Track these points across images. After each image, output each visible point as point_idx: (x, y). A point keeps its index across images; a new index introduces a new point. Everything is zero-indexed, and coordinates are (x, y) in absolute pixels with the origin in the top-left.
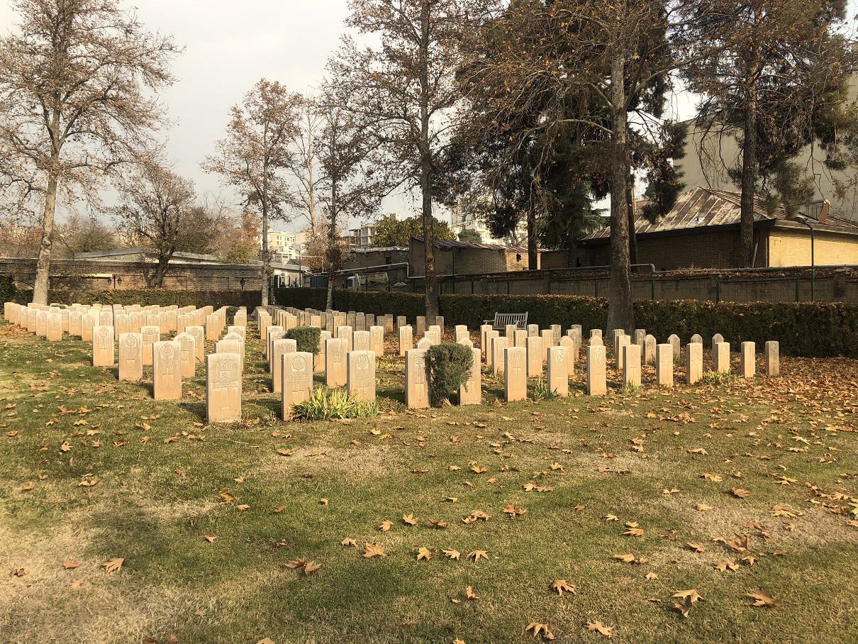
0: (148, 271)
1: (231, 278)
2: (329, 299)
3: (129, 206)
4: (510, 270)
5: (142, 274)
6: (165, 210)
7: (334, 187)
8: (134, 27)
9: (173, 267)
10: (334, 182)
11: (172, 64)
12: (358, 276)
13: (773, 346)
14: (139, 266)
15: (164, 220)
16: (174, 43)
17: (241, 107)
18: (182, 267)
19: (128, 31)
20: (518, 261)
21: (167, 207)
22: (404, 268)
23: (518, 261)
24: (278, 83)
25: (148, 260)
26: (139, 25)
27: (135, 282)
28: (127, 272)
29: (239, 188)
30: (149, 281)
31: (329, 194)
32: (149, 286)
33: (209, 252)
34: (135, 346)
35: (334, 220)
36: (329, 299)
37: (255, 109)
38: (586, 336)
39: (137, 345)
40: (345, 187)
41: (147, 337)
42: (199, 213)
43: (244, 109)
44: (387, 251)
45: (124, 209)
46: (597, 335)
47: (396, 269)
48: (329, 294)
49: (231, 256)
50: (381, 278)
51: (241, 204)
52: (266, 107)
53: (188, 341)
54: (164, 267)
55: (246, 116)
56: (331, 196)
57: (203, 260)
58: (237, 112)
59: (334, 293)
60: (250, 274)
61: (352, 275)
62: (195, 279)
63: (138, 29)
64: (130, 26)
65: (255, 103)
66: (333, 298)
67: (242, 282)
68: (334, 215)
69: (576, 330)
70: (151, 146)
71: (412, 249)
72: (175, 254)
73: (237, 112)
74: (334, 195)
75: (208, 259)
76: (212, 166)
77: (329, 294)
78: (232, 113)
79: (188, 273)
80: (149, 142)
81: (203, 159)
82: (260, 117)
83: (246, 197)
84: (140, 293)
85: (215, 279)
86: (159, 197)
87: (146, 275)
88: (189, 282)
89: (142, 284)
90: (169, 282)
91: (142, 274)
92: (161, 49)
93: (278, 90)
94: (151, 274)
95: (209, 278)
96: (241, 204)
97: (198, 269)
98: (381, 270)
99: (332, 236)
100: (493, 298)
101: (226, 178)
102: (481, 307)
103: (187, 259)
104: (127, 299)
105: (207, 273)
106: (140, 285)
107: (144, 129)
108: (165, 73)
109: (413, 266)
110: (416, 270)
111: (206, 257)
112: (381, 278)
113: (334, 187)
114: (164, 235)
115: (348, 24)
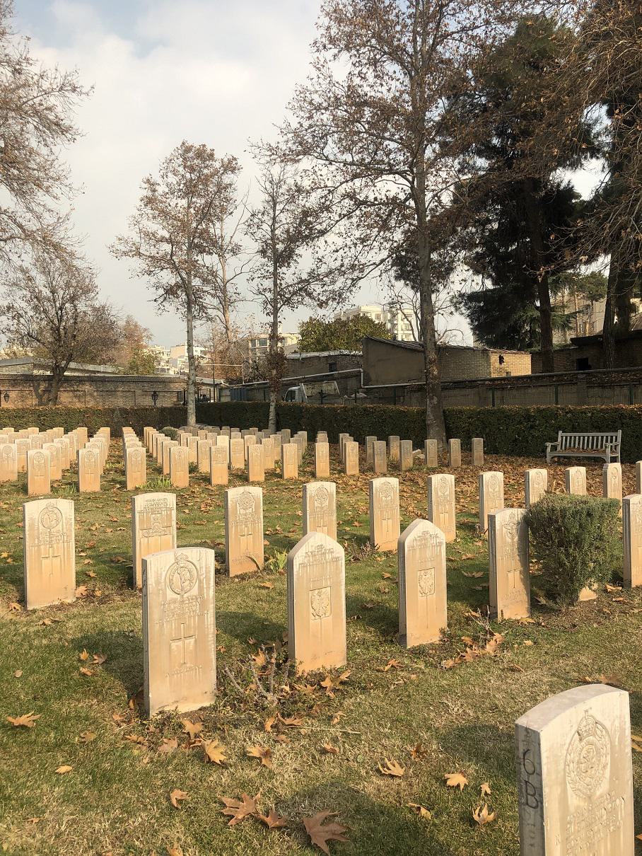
0: (39, 385)
1: (138, 392)
2: (272, 415)
3: (15, 305)
4: (493, 376)
5: (31, 389)
6: (61, 309)
7: (275, 275)
8: (24, 65)
9: (68, 379)
10: (276, 269)
11: (73, 111)
12: (303, 386)
13: (478, 443)
14: (28, 379)
15: (60, 321)
16: (79, 81)
17: (156, 178)
18: (80, 381)
19: (17, 71)
20: (500, 363)
21: (64, 304)
22: (357, 375)
23: (500, 363)
24: (204, 146)
25: (35, 372)
26: (31, 62)
27: (23, 398)
28: (13, 386)
29: (153, 280)
30: (40, 397)
31: (269, 283)
32: (41, 404)
33: (103, 362)
34: (195, 591)
35: (276, 317)
36: (272, 415)
37: (172, 179)
38: (312, 439)
39: (201, 589)
40: (289, 275)
41: (149, 519)
42: (100, 312)
43: (159, 181)
44: (330, 356)
45: (9, 308)
46: (322, 436)
47: (347, 377)
48: (272, 409)
49: (133, 367)
50: (329, 388)
51: (155, 300)
52: (188, 175)
53: (329, 557)
54: (57, 379)
55: (161, 189)
56: (272, 286)
57: (98, 372)
58: (151, 184)
59: (278, 407)
60: (159, 387)
61: (295, 385)
62: (95, 394)
63: (30, 68)
64: (19, 63)
65: (175, 173)
66: (277, 415)
67: (155, 395)
68: (275, 312)
69: (303, 434)
70: (49, 219)
71: (366, 351)
72: (72, 365)
73: (151, 184)
74: (275, 285)
75: (106, 369)
76: (124, 249)
77: (272, 409)
78: (146, 186)
79: (87, 387)
80: (46, 215)
81: (113, 241)
82: (180, 190)
83: (161, 291)
84: (33, 412)
85: (119, 394)
86: (53, 292)
87: (36, 390)
88: (88, 398)
89: (32, 402)
90: (66, 398)
91: (31, 389)
92: (61, 89)
93: (204, 155)
94: (42, 388)
95: (112, 393)
96: (155, 300)
97: (94, 380)
98: (330, 378)
99: (274, 337)
100: (539, 411)
101: (138, 264)
102: (520, 423)
103: (88, 371)
104: (18, 421)
105: (110, 386)
106: (29, 402)
107: (41, 196)
108: (66, 123)
109: (368, 374)
110: (373, 377)
111: (101, 368)
112: (329, 388)
113: (275, 275)
114: (59, 340)
115: (316, 48)
